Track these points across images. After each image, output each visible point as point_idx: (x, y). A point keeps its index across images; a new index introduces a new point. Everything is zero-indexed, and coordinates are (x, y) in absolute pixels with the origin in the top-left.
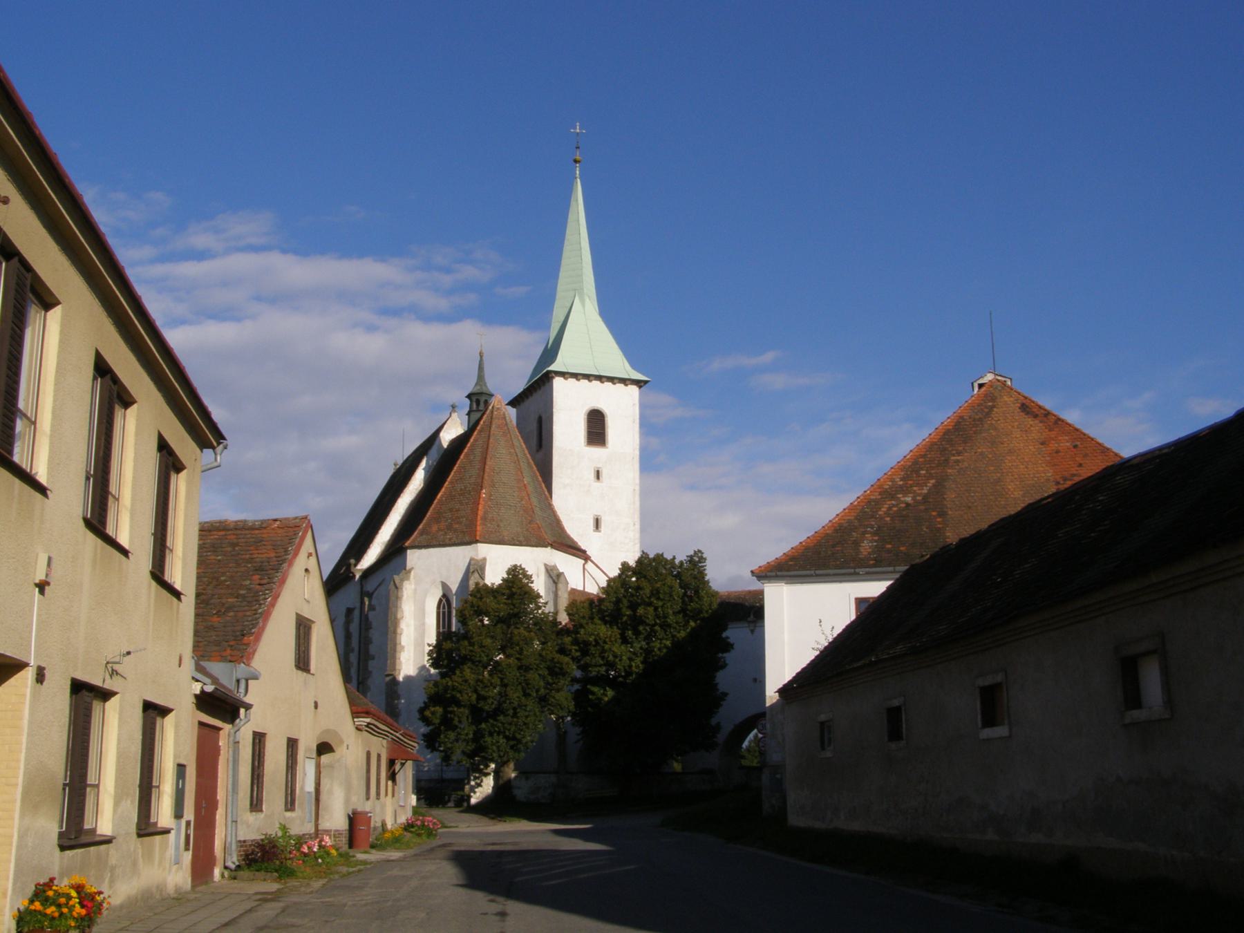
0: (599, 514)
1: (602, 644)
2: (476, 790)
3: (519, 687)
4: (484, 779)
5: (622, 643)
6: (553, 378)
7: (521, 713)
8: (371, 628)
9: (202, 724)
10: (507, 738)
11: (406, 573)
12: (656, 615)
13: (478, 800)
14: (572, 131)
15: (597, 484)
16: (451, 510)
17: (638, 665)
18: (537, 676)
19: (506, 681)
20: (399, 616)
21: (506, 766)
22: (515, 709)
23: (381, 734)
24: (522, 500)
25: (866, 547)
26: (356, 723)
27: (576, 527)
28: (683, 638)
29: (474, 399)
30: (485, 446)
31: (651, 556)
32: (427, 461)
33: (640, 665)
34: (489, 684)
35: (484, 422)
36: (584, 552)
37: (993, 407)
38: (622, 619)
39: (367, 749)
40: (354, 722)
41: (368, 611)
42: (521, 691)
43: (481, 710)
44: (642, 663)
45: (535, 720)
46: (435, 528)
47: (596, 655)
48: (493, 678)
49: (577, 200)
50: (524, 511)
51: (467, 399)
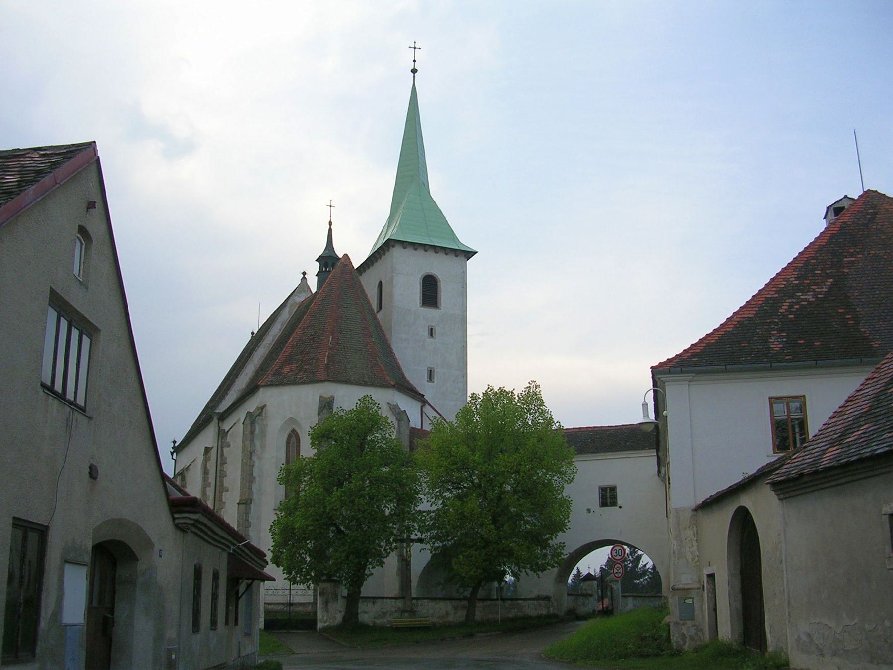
15: (432, 340)
23: (220, 543)
25: (775, 345)
26: (177, 521)
27: (415, 376)
37: (876, 214)
39: (196, 561)
40: (174, 519)
51: (317, 262)
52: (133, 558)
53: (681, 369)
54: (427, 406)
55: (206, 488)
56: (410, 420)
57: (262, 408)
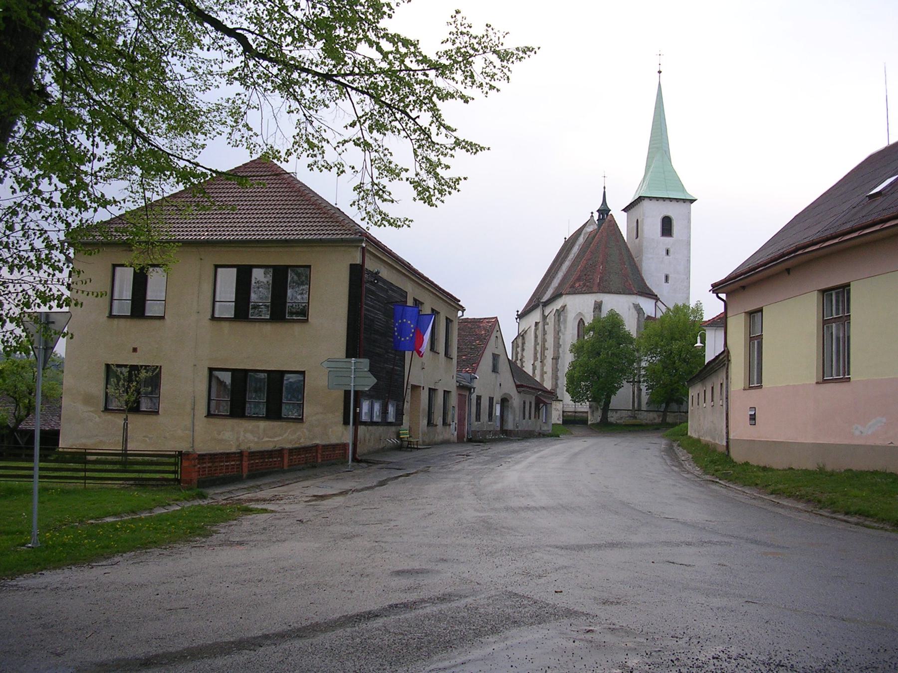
9: (459, 394)
15: (668, 257)
27: (653, 281)
52: (508, 401)
54: (659, 302)
57: (564, 307)
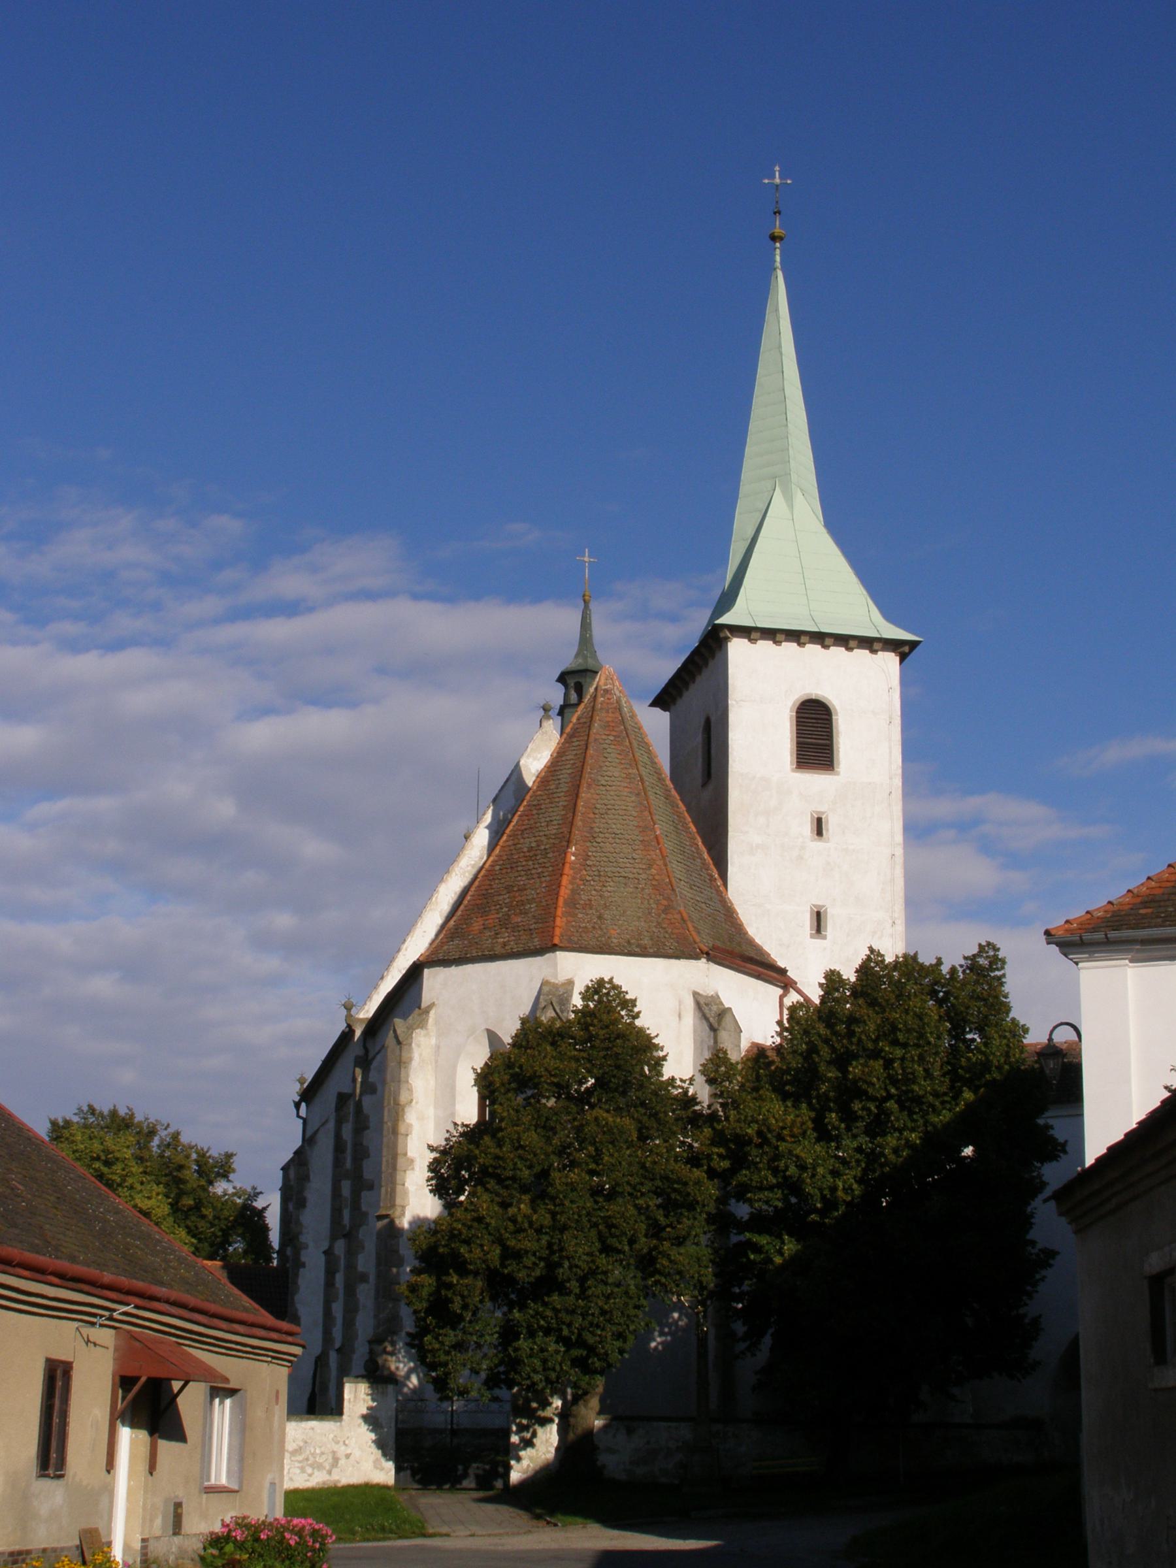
0: (820, 903)
1: (774, 1141)
2: (522, 1453)
3: (593, 1233)
4: (540, 1431)
5: (818, 1140)
6: (727, 639)
7: (594, 1288)
8: (367, 1128)
10: (566, 1342)
11: (420, 1015)
12: (890, 1077)
13: (524, 1476)
14: (766, 181)
15: (818, 845)
16: (509, 889)
17: (848, 1185)
18: (632, 1211)
19: (562, 1219)
20: (403, 1098)
21: (581, 1403)
22: (582, 1280)
24: (650, 867)
28: (946, 1126)
29: (571, 683)
30: (579, 764)
31: (889, 959)
32: (494, 811)
33: (855, 1186)
34: (526, 1225)
35: (578, 719)
36: (783, 972)
38: (818, 1089)
41: (361, 1095)
42: (595, 1239)
43: (510, 1280)
44: (860, 1181)
45: (626, 1304)
46: (477, 925)
47: (761, 1165)
48: (535, 1211)
49: (777, 310)
50: (655, 887)
53: (1106, 935)
55: (340, 1181)
56: (742, 1029)
